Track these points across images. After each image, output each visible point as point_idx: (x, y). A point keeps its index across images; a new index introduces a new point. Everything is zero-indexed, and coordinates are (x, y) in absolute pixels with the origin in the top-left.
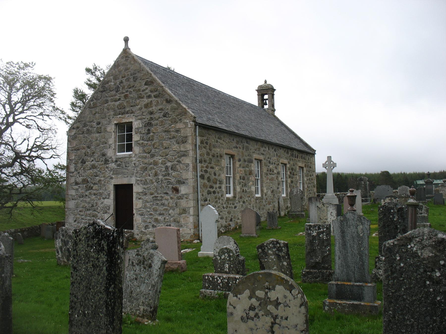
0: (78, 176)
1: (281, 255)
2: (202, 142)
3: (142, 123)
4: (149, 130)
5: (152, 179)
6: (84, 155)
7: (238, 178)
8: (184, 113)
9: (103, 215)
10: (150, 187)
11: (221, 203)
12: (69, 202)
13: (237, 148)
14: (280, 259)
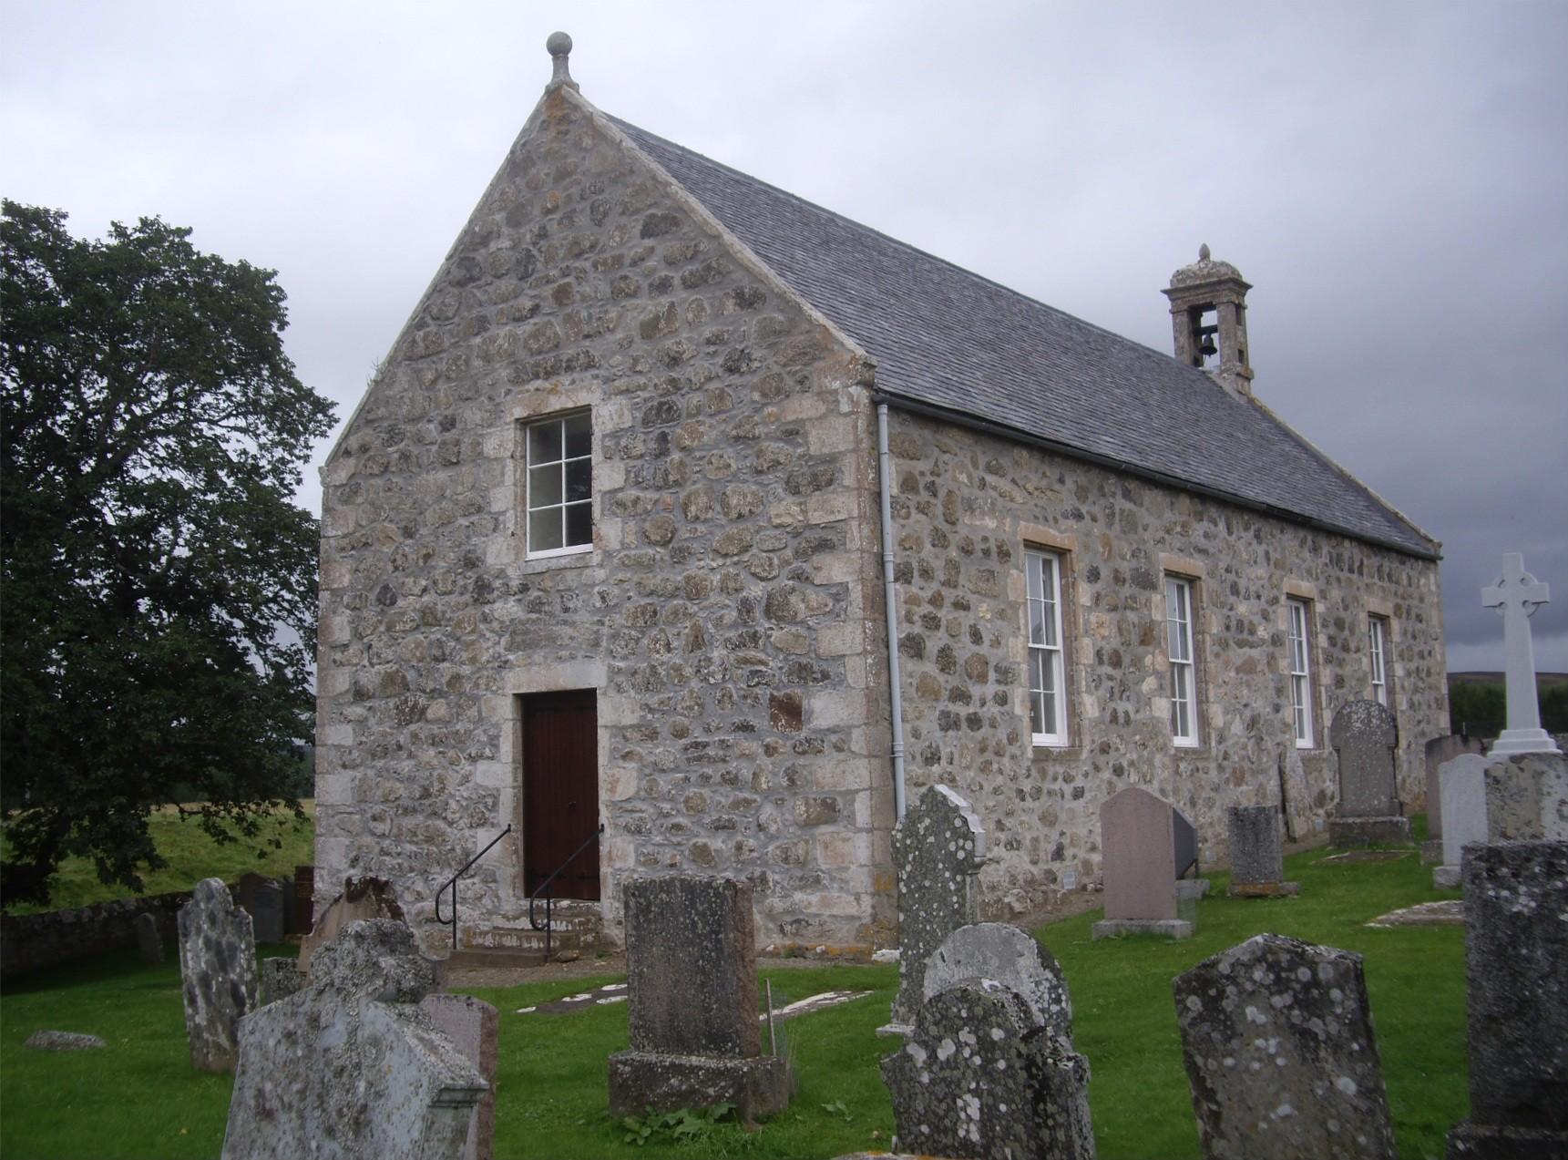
0: (366, 662)
1: (1322, 1037)
2: (908, 484)
3: (635, 407)
4: (663, 438)
5: (678, 661)
6: (390, 567)
7: (1087, 655)
8: (817, 349)
9: (467, 832)
10: (672, 703)
11: (1007, 770)
12: (330, 778)
13: (1078, 516)
14: (1317, 1059)
